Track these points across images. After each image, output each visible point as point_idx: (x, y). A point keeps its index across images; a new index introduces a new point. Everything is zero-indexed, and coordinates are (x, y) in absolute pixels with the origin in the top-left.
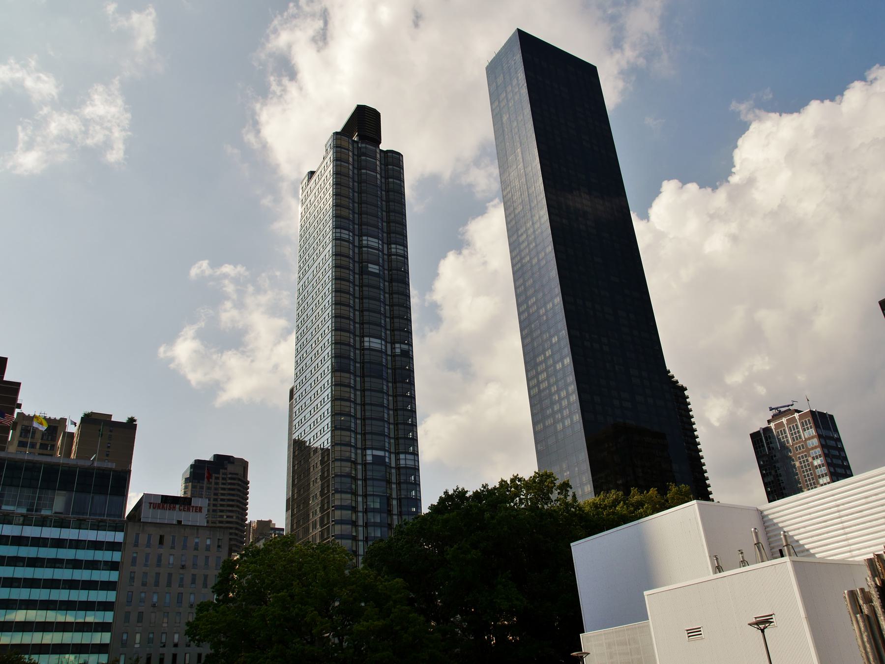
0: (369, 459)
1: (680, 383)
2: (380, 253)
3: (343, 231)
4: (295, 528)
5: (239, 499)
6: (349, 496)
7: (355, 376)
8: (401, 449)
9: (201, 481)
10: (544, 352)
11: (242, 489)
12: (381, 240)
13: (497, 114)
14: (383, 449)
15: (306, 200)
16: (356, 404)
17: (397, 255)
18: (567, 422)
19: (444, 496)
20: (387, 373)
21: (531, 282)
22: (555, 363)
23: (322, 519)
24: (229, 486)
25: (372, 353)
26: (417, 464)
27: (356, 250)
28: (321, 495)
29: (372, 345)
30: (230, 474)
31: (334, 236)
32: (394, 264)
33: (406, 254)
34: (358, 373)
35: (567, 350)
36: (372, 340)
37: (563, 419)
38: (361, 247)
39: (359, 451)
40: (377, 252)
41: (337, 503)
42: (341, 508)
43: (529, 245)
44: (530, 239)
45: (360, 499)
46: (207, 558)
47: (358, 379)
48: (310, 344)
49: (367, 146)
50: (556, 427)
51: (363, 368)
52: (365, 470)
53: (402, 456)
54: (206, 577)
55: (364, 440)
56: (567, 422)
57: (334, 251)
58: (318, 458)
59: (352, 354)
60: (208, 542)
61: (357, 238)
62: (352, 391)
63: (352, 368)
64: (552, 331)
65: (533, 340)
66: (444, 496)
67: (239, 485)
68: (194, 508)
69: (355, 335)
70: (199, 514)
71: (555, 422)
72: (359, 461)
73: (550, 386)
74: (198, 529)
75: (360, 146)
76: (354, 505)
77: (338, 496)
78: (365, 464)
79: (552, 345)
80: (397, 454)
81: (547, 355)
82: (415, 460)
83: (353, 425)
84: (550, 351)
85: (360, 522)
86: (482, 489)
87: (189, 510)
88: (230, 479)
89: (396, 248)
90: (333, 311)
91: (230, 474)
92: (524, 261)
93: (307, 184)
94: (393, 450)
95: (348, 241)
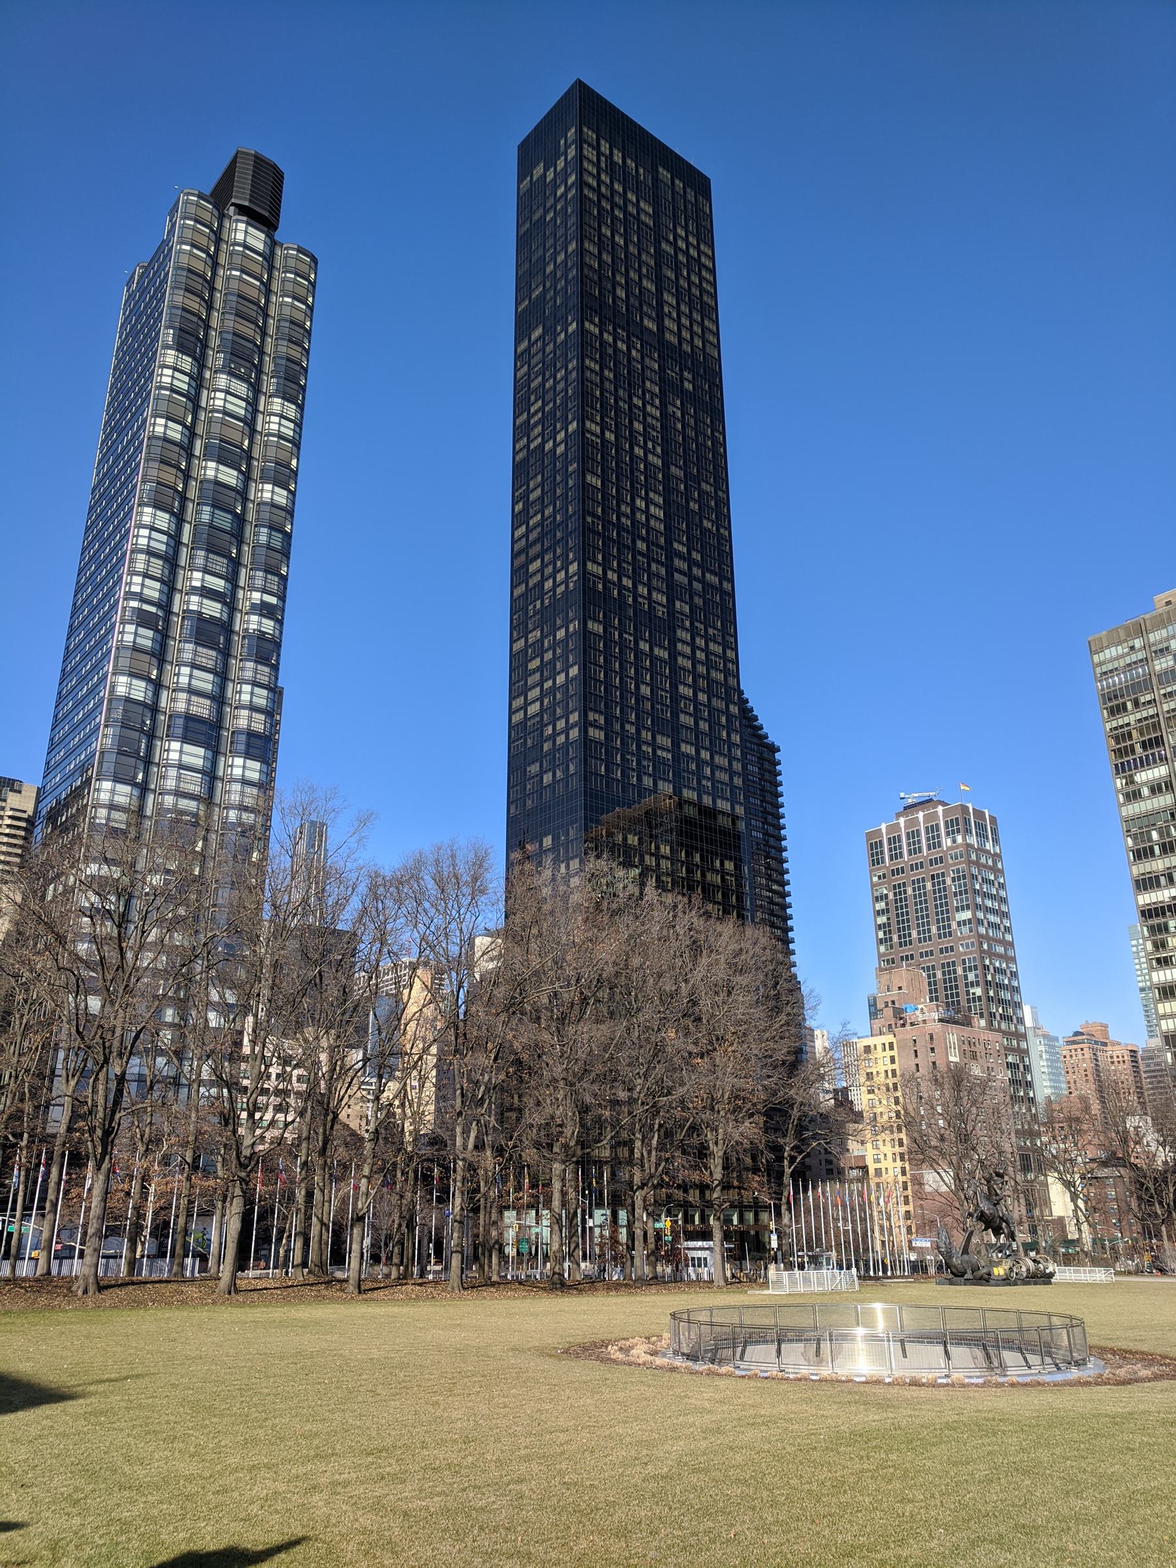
1: (771, 738)
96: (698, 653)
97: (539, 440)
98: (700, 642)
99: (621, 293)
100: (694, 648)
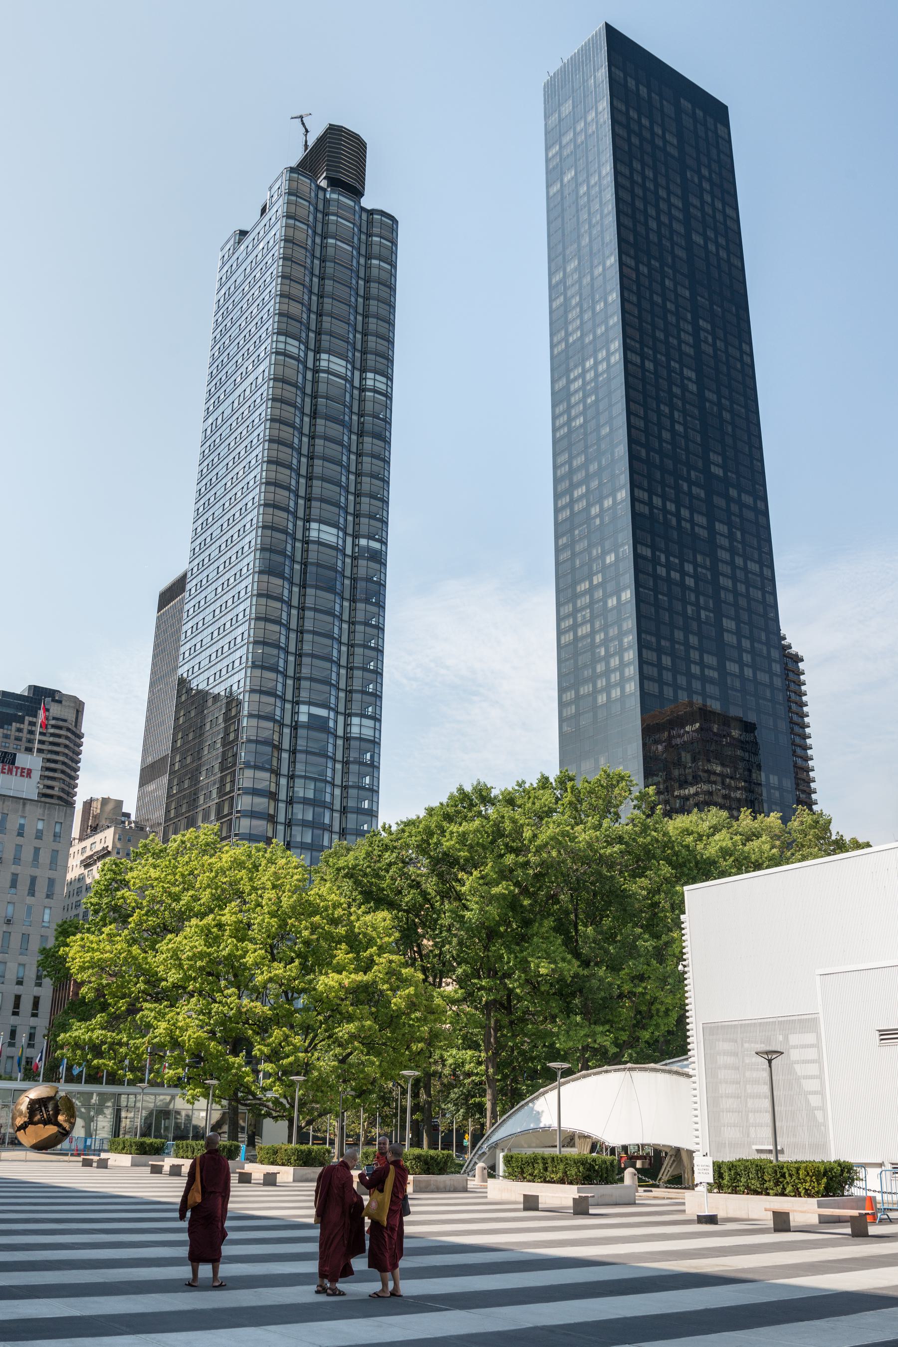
0: (303, 718)
1: (795, 649)
2: (348, 385)
3: (289, 340)
4: (172, 815)
5: (66, 760)
6: (266, 775)
7: (292, 584)
8: (356, 708)
9: (6, 726)
10: (590, 577)
11: (71, 745)
12: (350, 363)
13: (554, 168)
14: (325, 705)
15: (228, 279)
16: (289, 629)
17: (375, 391)
18: (616, 693)
19: (456, 794)
20: (343, 584)
21: (580, 460)
22: (606, 597)
23: (219, 807)
24: (51, 739)
25: (322, 549)
26: (377, 735)
27: (309, 375)
28: (222, 770)
29: (323, 535)
30: (54, 718)
31: (274, 346)
32: (369, 407)
33: (389, 390)
34: (297, 580)
35: (628, 578)
36: (324, 527)
37: (608, 689)
38: (316, 371)
39: (288, 706)
40: (343, 382)
41: (247, 784)
42: (254, 792)
43: (585, 397)
44: (588, 387)
45: (283, 781)
46: (37, 850)
47: (296, 589)
48: (220, 523)
49: (341, 198)
50: (595, 700)
51: (304, 572)
52: (294, 737)
53: (355, 720)
54: (33, 880)
55: (297, 689)
56: (616, 693)
57: (272, 373)
58: (221, 710)
59: (289, 548)
60: (40, 826)
61: (311, 355)
62: (285, 608)
63: (287, 570)
64: (607, 545)
65: (574, 555)
66: (456, 794)
67: (67, 738)
68: (19, 771)
69: (296, 517)
70: (26, 780)
71: (595, 692)
72: (287, 721)
73: (593, 633)
74: (24, 804)
75: (328, 196)
76: (273, 789)
77: (249, 773)
78: (295, 727)
79: (604, 569)
80: (348, 715)
81: (595, 582)
82: (375, 729)
83: (281, 663)
84: (600, 575)
85: (281, 818)
86: (517, 788)
87: (10, 771)
88: (53, 726)
89: (375, 380)
90: (264, 474)
91: (54, 718)
92: (573, 424)
93: (231, 251)
94: (341, 709)
95: (297, 359)
96: (738, 572)
97: (584, 503)
98: (739, 561)
99: (653, 224)
100: (734, 567)
